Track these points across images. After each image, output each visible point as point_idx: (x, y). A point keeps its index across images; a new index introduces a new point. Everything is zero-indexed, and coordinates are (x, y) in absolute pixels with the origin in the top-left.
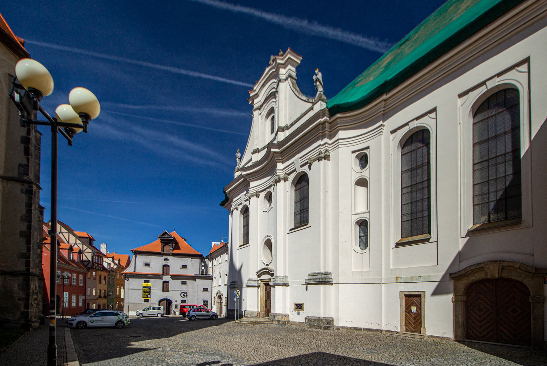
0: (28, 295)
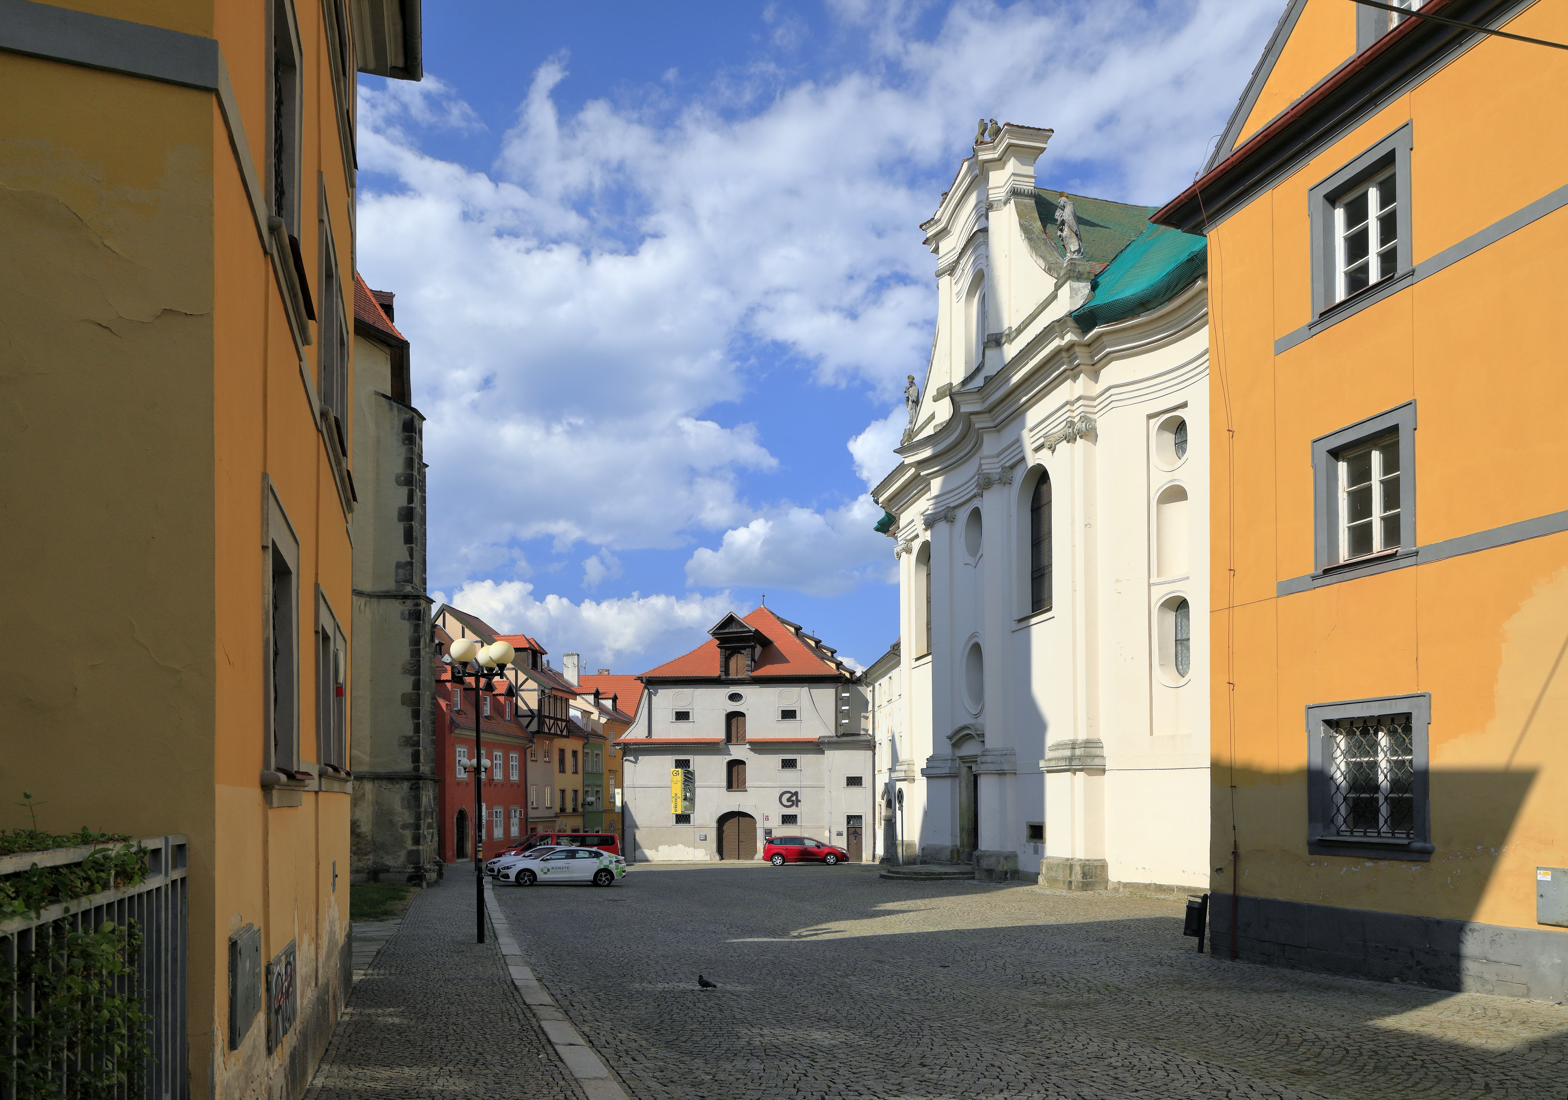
0: (418, 818)
